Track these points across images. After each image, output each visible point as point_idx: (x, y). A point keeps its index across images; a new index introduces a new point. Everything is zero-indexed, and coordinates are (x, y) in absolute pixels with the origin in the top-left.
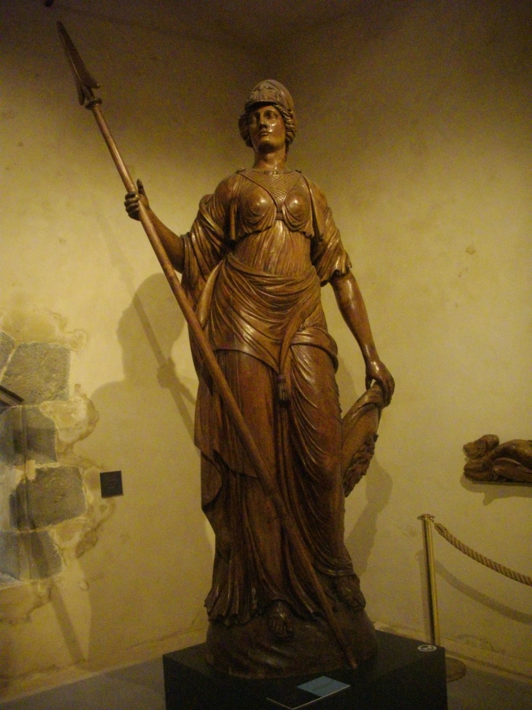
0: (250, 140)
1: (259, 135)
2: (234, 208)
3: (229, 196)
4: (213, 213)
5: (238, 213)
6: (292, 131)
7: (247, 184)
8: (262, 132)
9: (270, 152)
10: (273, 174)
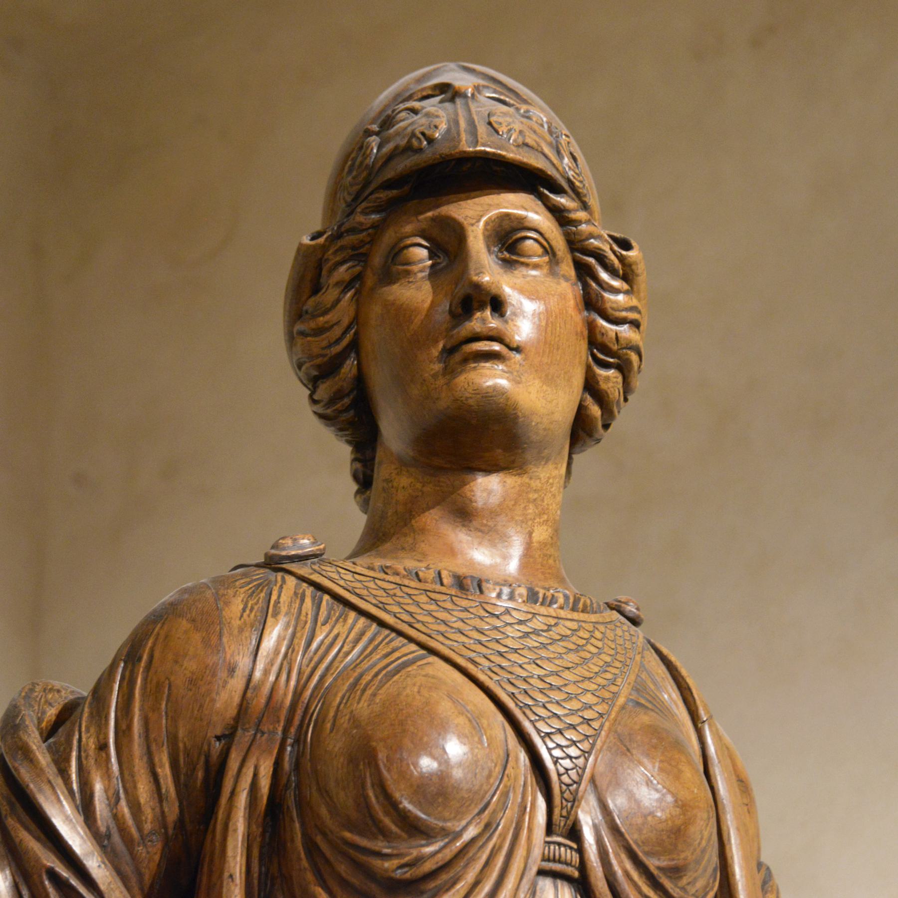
0: (360, 381)
1: (450, 351)
2: (251, 776)
3: (227, 696)
4: (98, 788)
5: (272, 816)
6: (624, 368)
7: (342, 641)
8: (477, 338)
9: (491, 469)
10: (499, 596)
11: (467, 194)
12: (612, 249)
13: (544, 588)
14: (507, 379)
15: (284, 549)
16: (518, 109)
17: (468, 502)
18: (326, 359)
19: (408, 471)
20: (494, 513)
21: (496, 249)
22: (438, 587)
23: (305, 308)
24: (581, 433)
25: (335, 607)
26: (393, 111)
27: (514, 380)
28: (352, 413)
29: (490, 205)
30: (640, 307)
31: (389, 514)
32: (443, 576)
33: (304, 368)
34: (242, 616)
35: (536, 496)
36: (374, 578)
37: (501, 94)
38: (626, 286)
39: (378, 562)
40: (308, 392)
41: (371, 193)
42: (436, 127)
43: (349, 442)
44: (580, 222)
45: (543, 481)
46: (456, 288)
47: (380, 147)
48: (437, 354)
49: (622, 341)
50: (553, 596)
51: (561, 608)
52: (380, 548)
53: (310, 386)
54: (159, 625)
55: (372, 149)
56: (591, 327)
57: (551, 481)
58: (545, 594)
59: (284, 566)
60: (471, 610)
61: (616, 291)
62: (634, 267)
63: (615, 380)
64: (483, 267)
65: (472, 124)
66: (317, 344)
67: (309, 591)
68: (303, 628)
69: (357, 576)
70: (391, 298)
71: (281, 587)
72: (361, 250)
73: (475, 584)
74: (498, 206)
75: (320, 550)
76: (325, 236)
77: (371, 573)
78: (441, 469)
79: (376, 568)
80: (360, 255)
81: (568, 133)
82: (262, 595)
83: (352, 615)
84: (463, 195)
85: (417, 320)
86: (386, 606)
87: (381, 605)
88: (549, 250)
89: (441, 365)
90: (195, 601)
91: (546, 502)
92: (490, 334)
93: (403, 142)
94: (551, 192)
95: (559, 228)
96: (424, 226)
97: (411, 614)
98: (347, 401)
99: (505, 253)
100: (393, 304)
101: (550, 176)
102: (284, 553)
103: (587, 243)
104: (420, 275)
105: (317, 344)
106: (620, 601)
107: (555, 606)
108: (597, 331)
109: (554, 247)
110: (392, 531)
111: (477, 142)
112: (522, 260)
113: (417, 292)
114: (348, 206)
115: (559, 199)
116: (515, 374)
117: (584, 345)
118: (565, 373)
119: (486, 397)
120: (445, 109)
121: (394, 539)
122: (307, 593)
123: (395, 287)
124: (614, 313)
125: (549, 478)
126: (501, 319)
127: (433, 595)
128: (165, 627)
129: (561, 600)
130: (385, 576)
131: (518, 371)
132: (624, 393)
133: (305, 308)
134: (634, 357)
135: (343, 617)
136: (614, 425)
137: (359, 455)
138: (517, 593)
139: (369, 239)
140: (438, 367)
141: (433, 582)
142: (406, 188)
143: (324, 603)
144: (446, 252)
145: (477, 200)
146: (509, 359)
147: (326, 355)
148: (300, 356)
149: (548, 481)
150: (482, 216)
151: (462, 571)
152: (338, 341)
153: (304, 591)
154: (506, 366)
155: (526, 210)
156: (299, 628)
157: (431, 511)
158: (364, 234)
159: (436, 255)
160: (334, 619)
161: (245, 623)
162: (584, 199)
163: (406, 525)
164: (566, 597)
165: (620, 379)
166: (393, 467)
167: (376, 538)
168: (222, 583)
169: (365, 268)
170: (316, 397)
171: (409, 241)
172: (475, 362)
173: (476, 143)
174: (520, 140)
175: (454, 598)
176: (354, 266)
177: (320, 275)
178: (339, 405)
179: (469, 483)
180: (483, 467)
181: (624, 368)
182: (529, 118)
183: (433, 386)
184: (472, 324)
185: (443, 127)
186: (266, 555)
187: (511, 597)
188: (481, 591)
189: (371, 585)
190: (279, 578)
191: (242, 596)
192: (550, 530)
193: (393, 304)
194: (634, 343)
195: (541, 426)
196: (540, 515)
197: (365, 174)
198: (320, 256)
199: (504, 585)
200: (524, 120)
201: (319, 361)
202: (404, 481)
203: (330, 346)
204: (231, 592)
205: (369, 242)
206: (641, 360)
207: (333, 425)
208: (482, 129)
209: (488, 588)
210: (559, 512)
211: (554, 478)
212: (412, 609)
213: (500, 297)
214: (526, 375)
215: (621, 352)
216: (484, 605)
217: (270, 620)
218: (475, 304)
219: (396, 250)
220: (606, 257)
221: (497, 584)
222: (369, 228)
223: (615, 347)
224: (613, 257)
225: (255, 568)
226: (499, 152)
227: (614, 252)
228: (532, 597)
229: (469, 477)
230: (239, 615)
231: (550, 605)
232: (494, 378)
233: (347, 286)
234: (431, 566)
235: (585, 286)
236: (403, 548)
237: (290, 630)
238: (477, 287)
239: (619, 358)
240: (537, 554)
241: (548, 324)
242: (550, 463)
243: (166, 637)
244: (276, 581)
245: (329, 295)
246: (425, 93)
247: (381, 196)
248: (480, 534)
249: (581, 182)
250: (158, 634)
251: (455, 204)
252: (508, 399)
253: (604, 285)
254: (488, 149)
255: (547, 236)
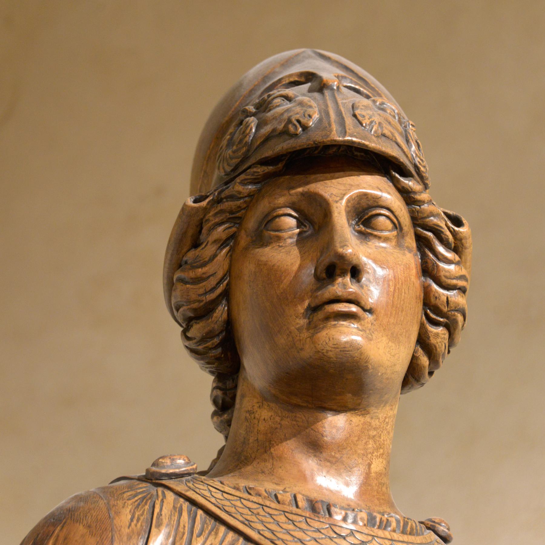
1: (314, 309)
6: (451, 327)
10: (345, 519)
11: (332, 174)
12: (446, 225)
13: (379, 513)
14: (362, 336)
15: (164, 467)
16: (374, 102)
17: (320, 436)
18: (202, 304)
19: (268, 405)
20: (341, 447)
21: (354, 223)
22: (294, 509)
23: (185, 259)
24: (411, 379)
25: (208, 521)
26: (269, 96)
27: (367, 338)
28: (219, 350)
29: (351, 185)
30: (467, 276)
31: (251, 441)
32: (298, 499)
33: (181, 310)
34: (130, 525)
35: (375, 433)
36: (240, 498)
37: (356, 84)
38: (457, 258)
39: (243, 483)
40: (182, 329)
41: (249, 167)
42: (310, 116)
43: (212, 373)
44: (423, 202)
45: (381, 420)
46: (321, 256)
47: (258, 127)
48: (302, 311)
49: (451, 305)
50: (387, 520)
51: (394, 531)
52: (243, 470)
53: (184, 325)
54: (59, 528)
55: (251, 129)
56: (427, 291)
57: (387, 420)
58: (381, 519)
59: (164, 482)
60: (322, 531)
61: (449, 262)
62: (463, 241)
63: (443, 336)
64: (346, 240)
65: (339, 114)
66: (195, 291)
67: (186, 505)
68: (182, 538)
69: (225, 495)
70: (264, 259)
71: (162, 501)
72: (237, 215)
73: (325, 507)
74: (358, 186)
75: (193, 469)
76: (207, 200)
77: (238, 493)
78: (298, 407)
79: (241, 488)
80: (236, 219)
81: (413, 124)
82: (147, 507)
83: (222, 529)
84: (328, 175)
85: (286, 281)
86: (252, 524)
87: (247, 522)
88: (397, 226)
89: (306, 321)
90: (90, 509)
91: (382, 438)
92: (350, 297)
93: (281, 127)
94: (401, 175)
95: (406, 207)
96: (294, 199)
97: (272, 532)
98: (216, 340)
99: (361, 226)
100: (266, 264)
101: (402, 163)
102: (164, 471)
103: (428, 220)
104: (289, 241)
105: (195, 291)
106: (434, 522)
107: (389, 529)
108: (432, 295)
109: (402, 223)
110: (253, 456)
111: (346, 132)
112: (376, 233)
113: (287, 255)
114: (227, 174)
115: (407, 182)
116: (368, 332)
117: (420, 306)
118: (407, 331)
119: (343, 351)
120: (315, 99)
121: (255, 463)
122: (183, 507)
123: (267, 250)
124: (446, 280)
125: (386, 418)
126: (357, 284)
127: (291, 516)
128: (65, 530)
129: (394, 524)
130: (249, 497)
131: (370, 330)
132: (449, 346)
133: (185, 259)
134: (460, 318)
135: (214, 531)
136: (436, 372)
137: (220, 385)
138: (359, 517)
139: (245, 206)
140: (303, 322)
141: (290, 504)
142: (280, 165)
143: (198, 517)
144: (312, 223)
145: (340, 180)
146: (364, 319)
147: (203, 301)
148: (179, 299)
149: (384, 420)
150: (344, 195)
151: (314, 495)
152: (213, 290)
153: (181, 506)
154: (361, 325)
155: (381, 190)
156: (177, 539)
157: (288, 442)
158: (242, 201)
159: (303, 224)
160: (207, 532)
161: (133, 531)
162: (426, 182)
163: (266, 452)
164: (398, 522)
165: (447, 336)
166: (255, 400)
167: (234, 459)
168: (110, 493)
169: (239, 230)
170: (189, 334)
171: (281, 211)
172: (335, 321)
173: (345, 133)
174: (380, 132)
175: (308, 520)
176: (230, 228)
177: (200, 232)
178: (209, 343)
179: (321, 420)
180: (335, 407)
181: (451, 327)
182: (384, 110)
183: (298, 338)
184: (335, 288)
185: (316, 116)
186: (147, 471)
187: (355, 522)
188: (330, 515)
189: (238, 504)
190: (160, 493)
191: (130, 507)
192: (384, 462)
193: (266, 264)
194: (461, 306)
195: (385, 376)
196: (377, 449)
197: (244, 149)
198: (202, 217)
199: (348, 509)
200: (380, 112)
201: (195, 305)
202: (265, 414)
203: (206, 293)
204: (120, 503)
205: (245, 208)
206: (465, 320)
207: (202, 359)
208: (349, 121)
209: (336, 513)
210: (391, 446)
211: (390, 417)
212: (274, 527)
213: (359, 266)
214: (376, 333)
215: (450, 313)
216: (333, 527)
217: (154, 530)
218: (338, 271)
219: (270, 218)
220: (442, 232)
221: (342, 508)
222: (246, 197)
223: (445, 309)
224: (448, 233)
225: (138, 482)
226: (363, 141)
227: (449, 228)
228: (371, 521)
229: (321, 415)
230: (128, 524)
231: (385, 529)
232: (349, 334)
233: (223, 243)
234: (287, 490)
235: (424, 256)
236: (263, 472)
237: (171, 540)
238: (342, 257)
239: (447, 318)
240: (374, 483)
241: (393, 287)
242: (388, 405)
243: (65, 539)
244: (157, 495)
245: (208, 251)
246: (292, 79)
247: (259, 170)
248: (328, 464)
249: (424, 167)
250: (58, 536)
251: (321, 182)
252: (361, 354)
253: (440, 257)
254: (354, 139)
255: (397, 213)
